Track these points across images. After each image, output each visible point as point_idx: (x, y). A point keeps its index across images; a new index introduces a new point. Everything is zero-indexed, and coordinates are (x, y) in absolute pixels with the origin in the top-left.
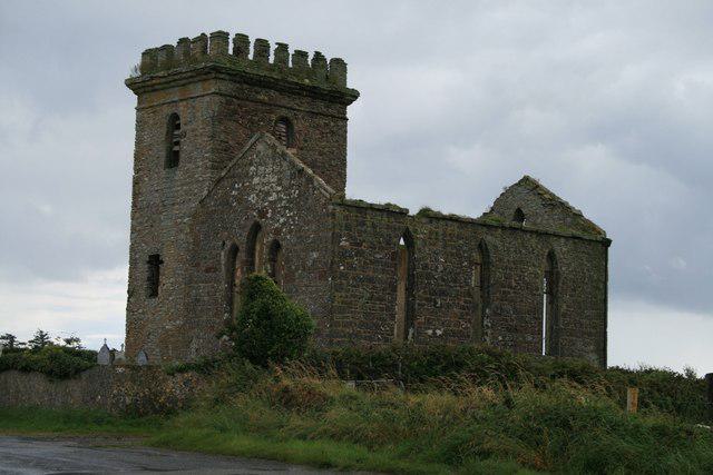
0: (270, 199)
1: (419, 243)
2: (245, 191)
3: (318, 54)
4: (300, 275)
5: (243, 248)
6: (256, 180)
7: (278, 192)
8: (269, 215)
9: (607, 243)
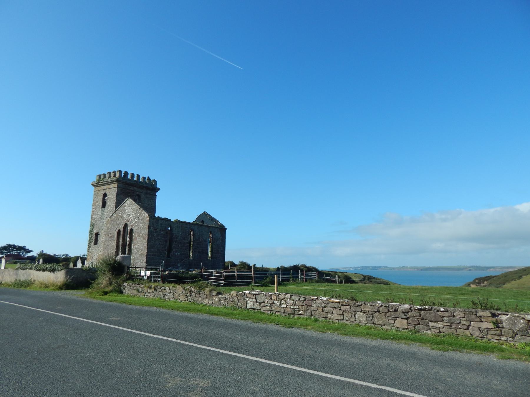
0: (130, 216)
2: (123, 214)
5: (122, 230)
6: (127, 211)
7: (133, 215)
8: (130, 221)
9: (226, 229)
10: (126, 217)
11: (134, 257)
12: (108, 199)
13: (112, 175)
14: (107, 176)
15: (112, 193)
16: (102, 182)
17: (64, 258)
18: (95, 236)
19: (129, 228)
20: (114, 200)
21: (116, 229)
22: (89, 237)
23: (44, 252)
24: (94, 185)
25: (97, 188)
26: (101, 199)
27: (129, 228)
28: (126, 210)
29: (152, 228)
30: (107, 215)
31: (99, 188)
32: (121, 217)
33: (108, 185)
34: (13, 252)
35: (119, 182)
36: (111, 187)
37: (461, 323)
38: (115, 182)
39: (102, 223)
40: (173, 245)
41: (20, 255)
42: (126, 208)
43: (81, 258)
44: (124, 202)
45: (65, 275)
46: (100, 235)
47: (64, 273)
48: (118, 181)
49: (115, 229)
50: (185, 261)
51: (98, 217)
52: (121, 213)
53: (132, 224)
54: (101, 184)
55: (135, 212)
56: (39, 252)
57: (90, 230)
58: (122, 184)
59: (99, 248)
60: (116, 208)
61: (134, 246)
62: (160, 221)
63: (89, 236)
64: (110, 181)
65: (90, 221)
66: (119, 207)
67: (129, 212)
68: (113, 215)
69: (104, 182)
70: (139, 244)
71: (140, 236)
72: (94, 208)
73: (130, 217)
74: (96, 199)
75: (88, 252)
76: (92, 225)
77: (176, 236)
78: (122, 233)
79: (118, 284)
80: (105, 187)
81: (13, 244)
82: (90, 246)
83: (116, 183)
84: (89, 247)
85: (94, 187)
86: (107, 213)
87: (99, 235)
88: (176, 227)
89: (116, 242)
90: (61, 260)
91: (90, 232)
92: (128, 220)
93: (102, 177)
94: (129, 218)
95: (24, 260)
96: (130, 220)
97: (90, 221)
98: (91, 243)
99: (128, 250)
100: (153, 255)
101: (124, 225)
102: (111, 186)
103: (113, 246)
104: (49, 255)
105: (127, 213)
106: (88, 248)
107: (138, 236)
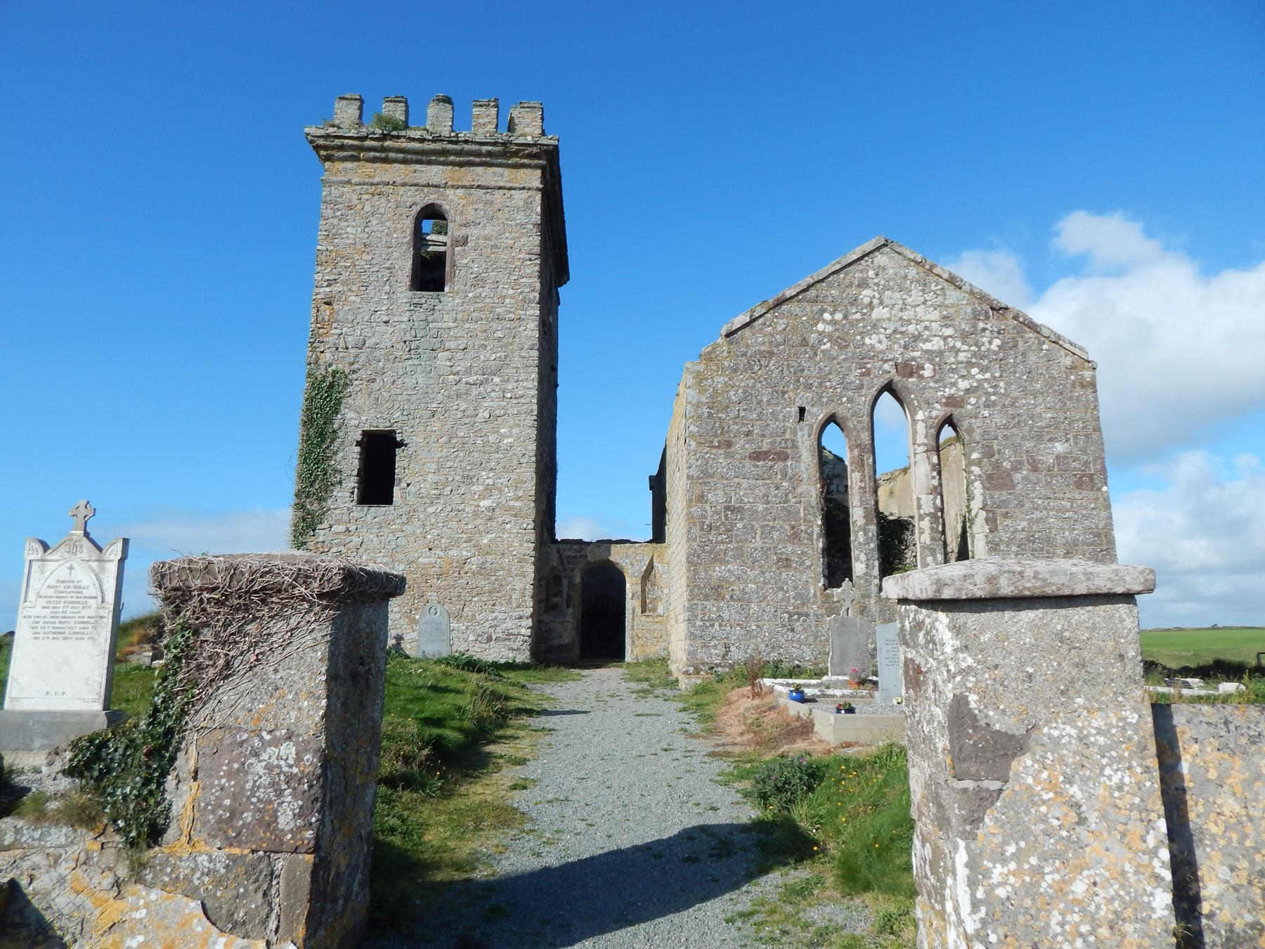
6: (879, 313)
7: (945, 339)
16: (422, 140)
25: (349, 165)
28: (871, 306)
33: (461, 165)
37: (1233, 921)
38: (530, 156)
46: (409, 450)
49: (794, 410)
52: (827, 316)
55: (966, 327)
64: (495, 144)
68: (753, 321)
79: (817, 776)
83: (536, 167)
96: (928, 366)
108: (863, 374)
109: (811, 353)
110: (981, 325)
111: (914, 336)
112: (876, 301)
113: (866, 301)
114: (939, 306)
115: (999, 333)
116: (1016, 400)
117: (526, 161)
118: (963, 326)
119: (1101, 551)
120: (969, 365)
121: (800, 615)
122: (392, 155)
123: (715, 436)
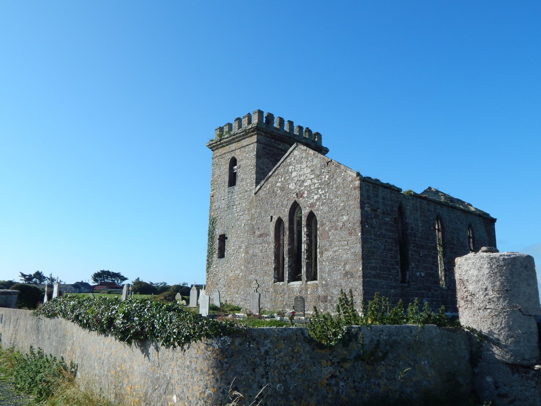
0: (305, 184)
1: (408, 213)
2: (286, 182)
3: (307, 128)
4: (333, 234)
5: (286, 219)
6: (294, 174)
7: (311, 179)
8: (305, 195)
9: (494, 221)
10: (293, 188)
11: (326, 281)
12: (239, 167)
13: (245, 122)
14: (235, 125)
15: (247, 155)
16: (228, 138)
17: (162, 287)
18: (218, 241)
19: (305, 212)
20: (252, 167)
21: (272, 217)
22: (208, 245)
23: (140, 280)
24: (212, 145)
26: (227, 170)
27: (305, 212)
28: (291, 172)
29: (368, 207)
30: (240, 199)
31: (220, 150)
32: (282, 189)
33: (239, 141)
34: (107, 280)
35: (260, 132)
36: (245, 144)
38: (252, 132)
39: (230, 216)
40: (410, 252)
41: (115, 284)
42: (291, 167)
43: (196, 286)
44: (287, 154)
45: (209, 379)
46: (228, 239)
47: (203, 365)
48: (258, 129)
49: (270, 217)
50: (435, 293)
51: (223, 204)
52: (280, 180)
53: (312, 201)
54: (225, 142)
55: (318, 173)
56: (135, 280)
57: (210, 231)
58: (265, 136)
59: (228, 265)
60: (257, 183)
61: (322, 253)
62: (381, 189)
63: (208, 242)
65: (207, 213)
66: (275, 168)
67: (300, 176)
69: (230, 137)
70: (336, 249)
71: (339, 228)
72: (213, 190)
73: (306, 186)
74: (217, 172)
75: (208, 272)
76: (213, 222)
77: (412, 229)
78: (287, 225)
80: (233, 146)
81: (107, 270)
82: (210, 260)
84: (209, 264)
85: (212, 150)
86: (240, 194)
87: (227, 238)
88: (410, 207)
89: (275, 246)
90: (158, 290)
91: (209, 234)
92: (299, 195)
93: (226, 129)
94: (303, 188)
95: (119, 290)
96: (306, 192)
97: (208, 213)
98: (212, 254)
99: (307, 263)
100: (375, 276)
101: (289, 207)
102: (245, 142)
103: (267, 256)
104: (146, 283)
105: (296, 179)
106: (208, 264)
107: (332, 227)
108: (288, 200)
109: (275, 195)
110: (323, 170)
111: (302, 181)
112: (293, 170)
113: (290, 170)
114: (311, 166)
115: (328, 172)
116: (332, 200)
117: (252, 134)
118: (317, 173)
119: (357, 262)
120: (318, 188)
121: (267, 292)
122: (224, 144)
123: (251, 231)
